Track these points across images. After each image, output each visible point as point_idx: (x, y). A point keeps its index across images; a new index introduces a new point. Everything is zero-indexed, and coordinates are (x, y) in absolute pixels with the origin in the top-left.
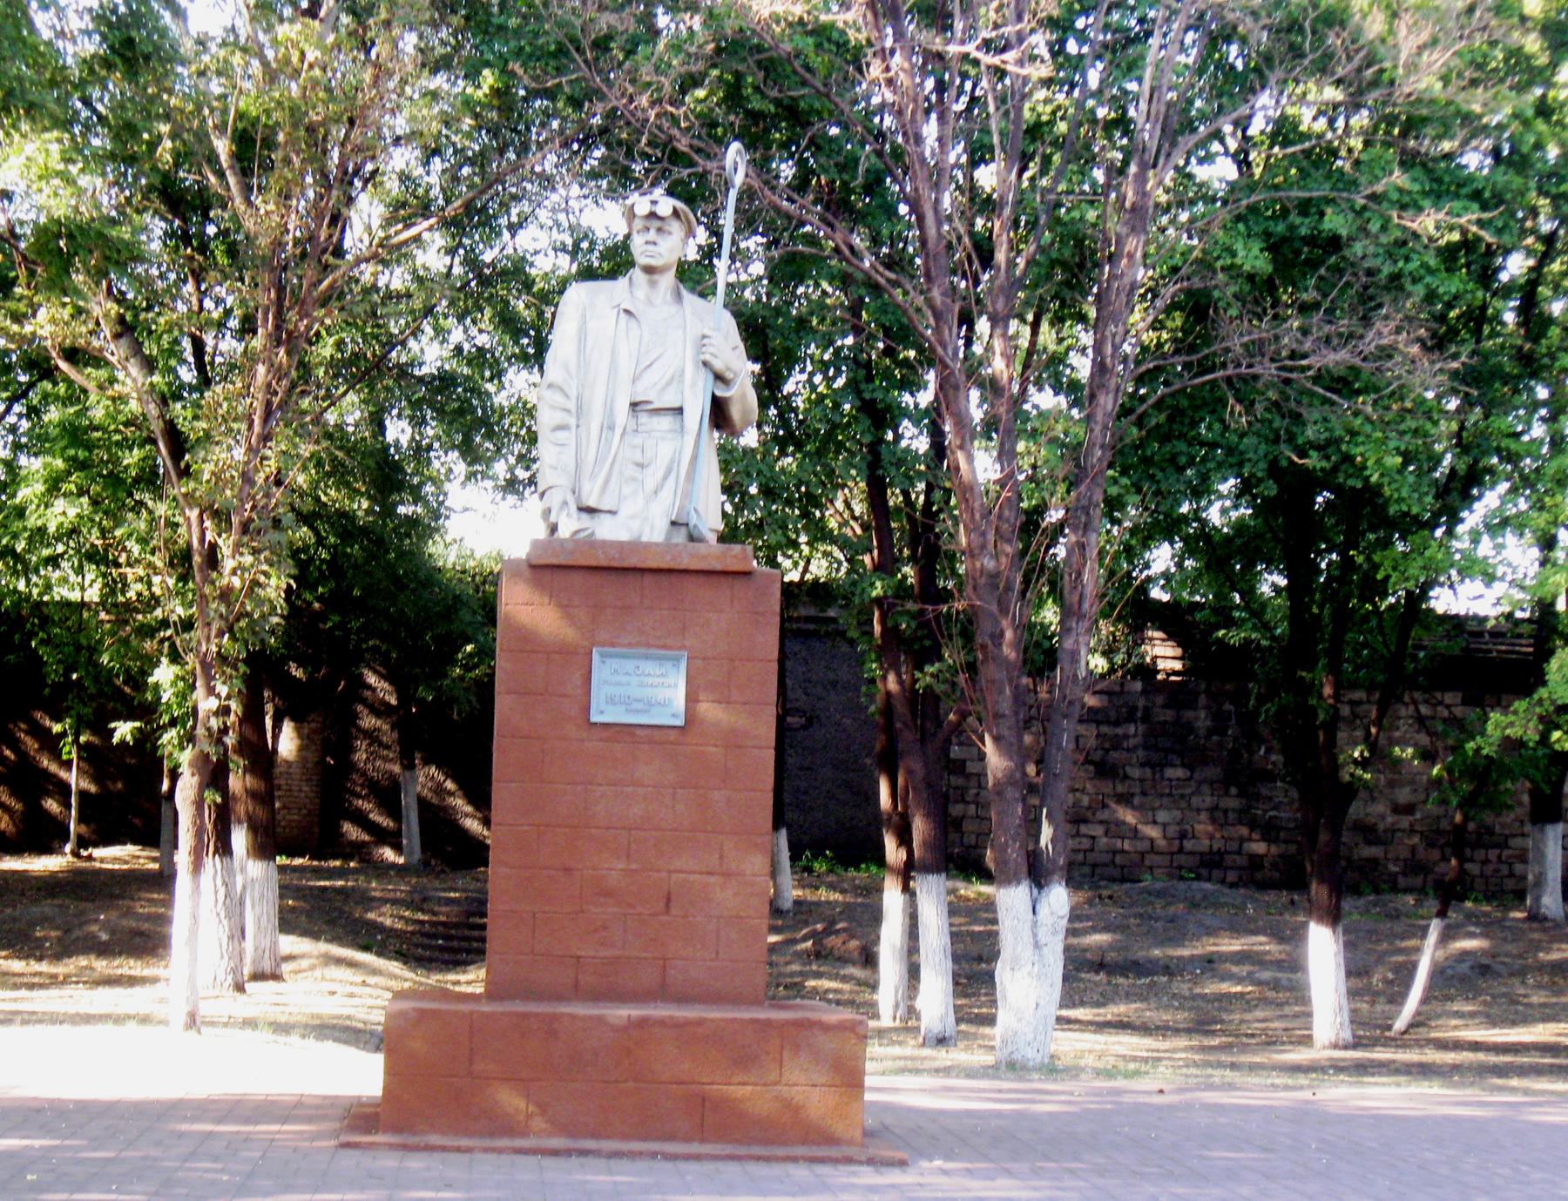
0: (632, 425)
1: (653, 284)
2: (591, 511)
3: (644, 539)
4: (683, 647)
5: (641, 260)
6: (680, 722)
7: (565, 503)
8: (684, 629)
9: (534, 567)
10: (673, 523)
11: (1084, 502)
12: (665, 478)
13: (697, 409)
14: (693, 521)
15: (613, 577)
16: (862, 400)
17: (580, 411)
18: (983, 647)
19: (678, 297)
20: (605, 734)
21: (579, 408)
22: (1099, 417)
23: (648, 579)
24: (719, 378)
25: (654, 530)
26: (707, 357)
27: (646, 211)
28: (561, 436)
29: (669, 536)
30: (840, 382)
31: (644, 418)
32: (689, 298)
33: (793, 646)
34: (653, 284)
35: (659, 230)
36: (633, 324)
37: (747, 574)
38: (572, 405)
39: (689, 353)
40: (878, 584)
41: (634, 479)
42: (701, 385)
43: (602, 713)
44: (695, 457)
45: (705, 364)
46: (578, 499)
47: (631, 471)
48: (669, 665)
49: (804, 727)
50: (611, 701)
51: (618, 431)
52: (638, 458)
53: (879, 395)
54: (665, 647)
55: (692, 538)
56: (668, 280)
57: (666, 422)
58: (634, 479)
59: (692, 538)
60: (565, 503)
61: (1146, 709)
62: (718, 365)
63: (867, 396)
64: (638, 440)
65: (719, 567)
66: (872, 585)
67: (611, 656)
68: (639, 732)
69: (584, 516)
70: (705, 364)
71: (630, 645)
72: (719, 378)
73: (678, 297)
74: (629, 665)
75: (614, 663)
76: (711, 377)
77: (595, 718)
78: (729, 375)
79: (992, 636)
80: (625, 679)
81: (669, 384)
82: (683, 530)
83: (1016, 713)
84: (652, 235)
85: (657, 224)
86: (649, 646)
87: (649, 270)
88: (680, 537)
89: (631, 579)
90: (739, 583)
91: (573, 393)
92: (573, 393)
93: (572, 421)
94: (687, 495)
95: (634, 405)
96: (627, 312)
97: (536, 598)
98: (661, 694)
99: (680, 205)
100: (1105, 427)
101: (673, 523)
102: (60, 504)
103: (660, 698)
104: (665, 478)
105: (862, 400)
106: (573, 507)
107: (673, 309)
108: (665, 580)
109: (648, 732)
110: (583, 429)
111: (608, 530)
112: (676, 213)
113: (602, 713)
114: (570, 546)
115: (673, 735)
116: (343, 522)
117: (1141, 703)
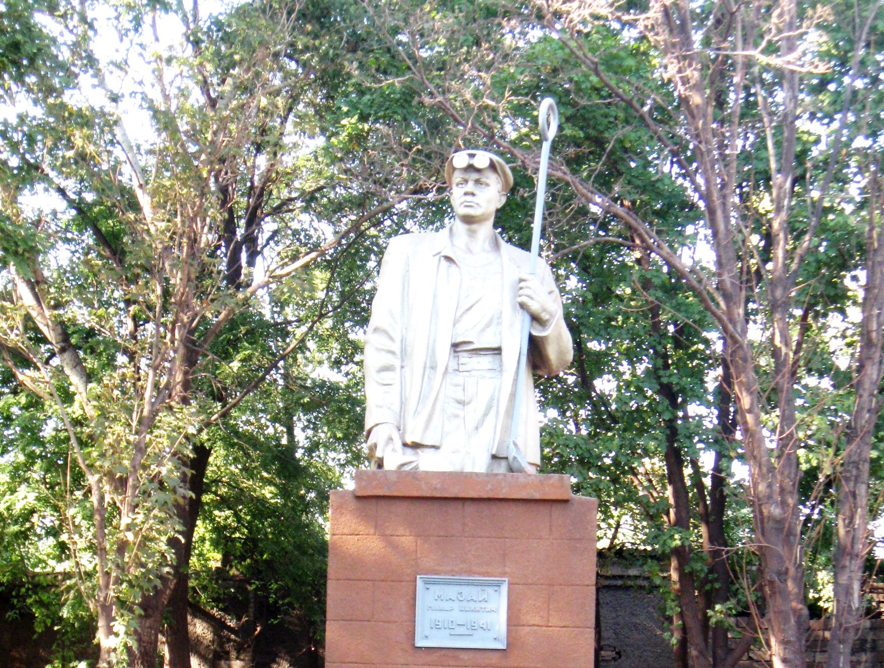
0: (453, 365)
1: (472, 233)
2: (416, 446)
3: (468, 469)
4: (504, 574)
5: (461, 210)
6: (502, 646)
7: (391, 439)
8: (504, 556)
9: (358, 498)
10: (494, 457)
11: (855, 458)
12: (486, 415)
13: (515, 348)
14: (512, 453)
15: (436, 505)
16: (661, 384)
17: (404, 353)
18: (771, 583)
19: (496, 246)
20: (429, 658)
21: (403, 351)
22: (867, 385)
23: (470, 508)
24: (535, 319)
25: (479, 464)
26: (524, 299)
27: (464, 164)
28: (387, 376)
29: (490, 466)
30: (641, 368)
31: (464, 358)
32: (509, 250)
33: (607, 597)
34: (472, 233)
35: (477, 182)
36: (453, 266)
37: (566, 501)
38: (396, 347)
39: (508, 296)
40: (677, 536)
41: (457, 416)
42: (518, 325)
43: (427, 636)
44: (513, 396)
45: (522, 306)
46: (402, 437)
47: (454, 408)
48: (490, 590)
49: (614, 659)
50: (436, 627)
51: (440, 370)
52: (460, 397)
53: (674, 380)
54: (487, 574)
55: (511, 470)
56: (486, 229)
57: (486, 362)
58: (457, 416)
59: (511, 470)
60: (391, 439)
61: (874, 641)
62: (535, 306)
63: (665, 380)
64: (459, 379)
65: (537, 496)
66: (672, 537)
67: (435, 583)
68: (464, 656)
69: (409, 451)
70: (522, 306)
71: (452, 572)
72: (535, 319)
73: (496, 246)
74: (452, 591)
75: (435, 590)
76: (528, 318)
77: (419, 643)
78: (545, 316)
79: (779, 574)
80: (446, 605)
81: (488, 326)
82: (504, 463)
83: (799, 640)
84: (470, 187)
85: (475, 176)
86: (470, 572)
87: (468, 220)
88: (501, 469)
89: (451, 508)
90: (557, 510)
91: (397, 337)
92: (397, 337)
93: (397, 363)
94: (507, 430)
95: (455, 346)
96: (448, 259)
97: (362, 528)
98: (483, 619)
99: (496, 158)
100: (872, 395)
101: (494, 457)
102: (23, 489)
103: (482, 622)
104: (486, 415)
105: (661, 384)
106: (398, 443)
107: (491, 256)
108: (485, 509)
109: (471, 654)
110: (407, 370)
111: (428, 462)
112: (493, 166)
113: (427, 636)
114: (393, 478)
115: (494, 659)
116: (260, 509)
117: (870, 638)
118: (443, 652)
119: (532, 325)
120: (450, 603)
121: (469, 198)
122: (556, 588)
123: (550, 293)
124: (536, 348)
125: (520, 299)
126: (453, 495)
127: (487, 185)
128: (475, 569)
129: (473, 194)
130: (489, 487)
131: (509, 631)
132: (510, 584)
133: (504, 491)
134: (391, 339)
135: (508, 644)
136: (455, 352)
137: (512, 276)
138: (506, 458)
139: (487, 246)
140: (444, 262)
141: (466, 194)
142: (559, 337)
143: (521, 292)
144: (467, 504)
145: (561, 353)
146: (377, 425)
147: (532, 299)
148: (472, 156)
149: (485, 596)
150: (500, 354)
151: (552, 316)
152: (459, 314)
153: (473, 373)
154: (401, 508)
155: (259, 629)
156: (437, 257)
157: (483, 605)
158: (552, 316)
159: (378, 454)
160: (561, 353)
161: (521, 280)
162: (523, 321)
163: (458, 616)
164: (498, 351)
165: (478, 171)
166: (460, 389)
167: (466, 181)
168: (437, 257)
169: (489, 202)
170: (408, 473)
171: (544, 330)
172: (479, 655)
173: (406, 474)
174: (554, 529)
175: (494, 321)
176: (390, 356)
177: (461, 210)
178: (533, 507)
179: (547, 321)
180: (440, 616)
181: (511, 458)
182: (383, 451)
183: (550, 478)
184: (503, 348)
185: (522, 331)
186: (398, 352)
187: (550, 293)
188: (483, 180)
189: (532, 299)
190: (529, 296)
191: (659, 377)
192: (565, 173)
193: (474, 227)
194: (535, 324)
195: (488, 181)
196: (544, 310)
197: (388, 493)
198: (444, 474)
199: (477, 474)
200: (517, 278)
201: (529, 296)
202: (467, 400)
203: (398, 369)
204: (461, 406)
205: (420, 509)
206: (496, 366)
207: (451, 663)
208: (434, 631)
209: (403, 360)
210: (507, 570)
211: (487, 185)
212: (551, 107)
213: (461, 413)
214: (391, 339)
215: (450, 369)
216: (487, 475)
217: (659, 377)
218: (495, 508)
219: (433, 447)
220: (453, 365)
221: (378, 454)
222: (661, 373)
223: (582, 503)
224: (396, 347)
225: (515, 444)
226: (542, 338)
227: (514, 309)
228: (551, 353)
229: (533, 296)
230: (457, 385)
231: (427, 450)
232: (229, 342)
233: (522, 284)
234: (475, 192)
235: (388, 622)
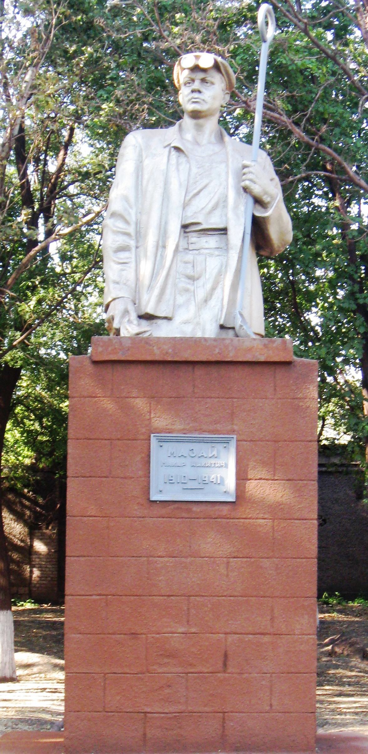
0: (183, 244)
1: (199, 128)
2: (148, 317)
4: (233, 431)
6: (232, 499)
8: (232, 414)
10: (222, 327)
14: (238, 322)
19: (221, 138)
20: (164, 511)
23: (199, 372)
24: (258, 201)
26: (247, 183)
28: (123, 255)
31: (193, 238)
34: (199, 128)
35: (203, 80)
36: (182, 156)
37: (288, 364)
38: (131, 230)
41: (187, 290)
45: (246, 190)
46: (137, 309)
47: (183, 283)
48: (220, 447)
52: (190, 272)
56: (211, 125)
57: (212, 241)
58: (187, 290)
62: (257, 190)
64: (189, 257)
68: (195, 508)
69: (144, 322)
70: (246, 190)
72: (258, 201)
75: (169, 447)
76: (251, 201)
78: (266, 199)
82: (231, 333)
84: (197, 85)
85: (201, 75)
86: (202, 431)
87: (196, 115)
89: (184, 373)
90: (280, 372)
93: (132, 243)
94: (232, 302)
95: (185, 227)
96: (177, 149)
99: (219, 59)
106: (133, 316)
107: (217, 148)
108: (214, 371)
110: (141, 249)
112: (217, 67)
114: (128, 344)
118: (176, 505)
119: (255, 207)
120: (182, 460)
121: (196, 95)
122: (280, 444)
123: (272, 180)
124: (259, 228)
125: (243, 184)
126: (184, 359)
127: (212, 83)
128: (204, 427)
129: (199, 92)
130: (217, 351)
131: (238, 485)
132: (237, 441)
133: (231, 354)
134: (127, 222)
135: (237, 497)
136: (185, 232)
137: (234, 163)
138: (233, 328)
139: (213, 139)
140: (173, 152)
141: (193, 91)
142: (280, 217)
143: (244, 177)
144: (198, 366)
145: (282, 233)
146: (114, 299)
147: (254, 183)
148: (197, 57)
149: (215, 453)
150: (226, 234)
151: (273, 198)
152: (188, 198)
153: (203, 251)
154: (135, 372)
155: (59, 506)
156: (167, 149)
157: (213, 461)
158: (273, 198)
159: (115, 325)
160: (282, 233)
161: (245, 167)
162: (246, 203)
163: (188, 471)
164: (224, 231)
165: (204, 70)
166: (190, 266)
167: (193, 80)
168: (167, 149)
169: (214, 98)
170: (143, 339)
171: (266, 212)
172: (209, 508)
173: (138, 340)
174: (278, 389)
175: (221, 204)
176: (125, 238)
177: (189, 107)
178: (258, 369)
179: (269, 203)
180: (173, 472)
181: (237, 328)
182: (120, 323)
183: (274, 342)
184: (228, 228)
185: (245, 212)
186: (133, 233)
187: (272, 180)
188: (209, 79)
189: (254, 183)
190: (251, 180)
191: (356, 299)
192: (281, 115)
193: (201, 121)
194: (258, 207)
195: (213, 80)
196: (266, 193)
197: (123, 358)
198: (174, 339)
199: (205, 339)
200: (240, 166)
201: (251, 180)
202: (196, 276)
203: (133, 249)
204: (191, 282)
205: (154, 372)
206: (222, 245)
207: (184, 515)
208: (169, 486)
209: (137, 241)
210: (236, 428)
211: (212, 83)
212: (268, 11)
213: (191, 288)
214: (127, 222)
215: (180, 249)
216: (215, 340)
217: (356, 299)
218: (223, 371)
219: (165, 318)
220: (183, 244)
221: (115, 325)
222: (358, 295)
223: (304, 364)
224: (131, 230)
225: (241, 315)
226: (264, 218)
227: (238, 193)
228: (273, 232)
229: (256, 180)
230: (186, 263)
231: (160, 322)
232: (28, 288)
233: (245, 170)
234: (201, 90)
235: (125, 478)
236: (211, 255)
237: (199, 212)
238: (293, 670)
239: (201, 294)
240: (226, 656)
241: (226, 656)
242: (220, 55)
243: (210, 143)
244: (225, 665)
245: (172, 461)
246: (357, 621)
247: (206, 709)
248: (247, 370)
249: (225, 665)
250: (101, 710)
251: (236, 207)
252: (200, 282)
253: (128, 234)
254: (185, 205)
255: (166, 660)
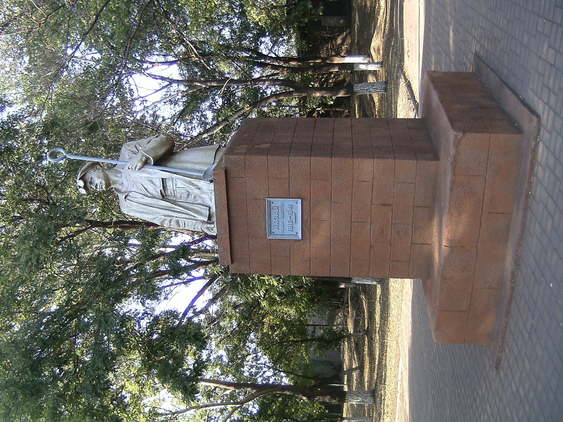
1: (115, 183)
2: (210, 217)
20: (307, 233)
23: (233, 214)
35: (91, 183)
58: (195, 197)
75: (274, 229)
118: (304, 227)
127: (92, 178)
129: (97, 185)
193: (111, 182)
196: (141, 159)
219: (209, 210)
236: (176, 185)
237: (156, 189)
238: (393, 172)
239: (197, 191)
240: (384, 205)
241: (384, 205)
242: (76, 170)
243: (121, 177)
244: (389, 205)
245: (281, 228)
246: (368, 348)
247: (412, 214)
248: (231, 191)
249: (389, 205)
250: (408, 263)
251: (150, 173)
252: (190, 191)
253: (170, 220)
254: (154, 197)
255: (385, 233)
